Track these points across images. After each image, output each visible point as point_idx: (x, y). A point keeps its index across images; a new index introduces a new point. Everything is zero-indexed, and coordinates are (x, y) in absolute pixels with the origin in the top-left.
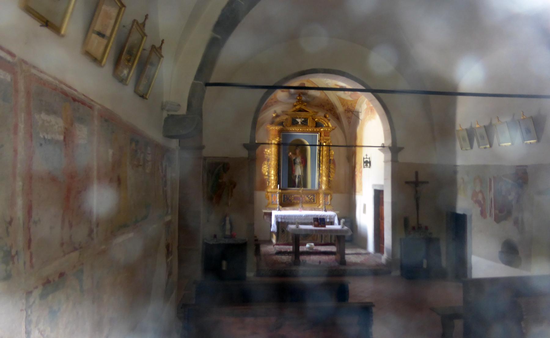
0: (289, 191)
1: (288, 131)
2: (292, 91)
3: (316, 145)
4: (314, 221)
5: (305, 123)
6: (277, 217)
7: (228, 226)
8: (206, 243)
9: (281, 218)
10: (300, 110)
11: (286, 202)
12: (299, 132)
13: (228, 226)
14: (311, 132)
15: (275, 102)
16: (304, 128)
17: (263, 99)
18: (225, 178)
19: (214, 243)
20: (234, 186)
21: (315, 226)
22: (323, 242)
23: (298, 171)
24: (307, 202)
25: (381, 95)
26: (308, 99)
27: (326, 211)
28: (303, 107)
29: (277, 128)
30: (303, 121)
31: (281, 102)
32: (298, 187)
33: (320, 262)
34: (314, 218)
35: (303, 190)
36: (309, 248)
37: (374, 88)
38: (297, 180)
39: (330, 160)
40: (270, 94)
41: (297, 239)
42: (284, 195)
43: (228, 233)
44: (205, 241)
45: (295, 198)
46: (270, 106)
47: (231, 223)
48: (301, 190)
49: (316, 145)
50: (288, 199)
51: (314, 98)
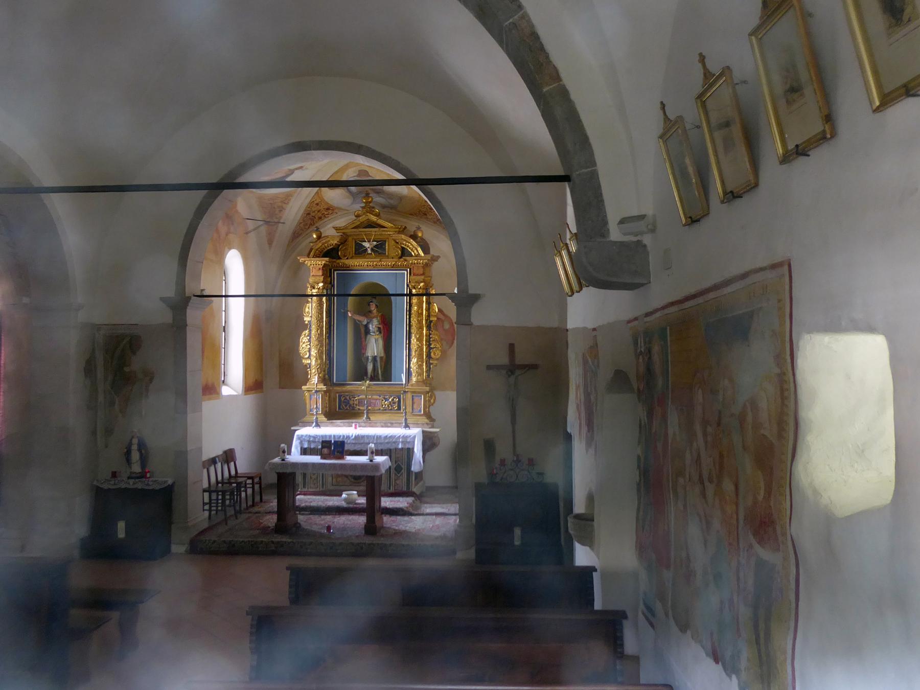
0: (348, 388)
1: (348, 268)
2: (353, 189)
3: (403, 295)
4: (323, 447)
5: (379, 249)
6: (300, 438)
7: (135, 456)
8: (98, 488)
9: (309, 441)
10: (372, 225)
11: (341, 409)
12: (375, 268)
13: (135, 456)
14: (394, 267)
15: (328, 209)
16: (375, 261)
17: (201, 211)
18: (136, 364)
19: (110, 487)
20: (151, 380)
21: (323, 458)
22: (392, 490)
23: (374, 347)
24: (385, 411)
25: (433, 188)
26: (392, 202)
27: (407, 426)
28: (374, 218)
29: (322, 262)
30: (375, 246)
31: (340, 209)
32: (372, 379)
33: (329, 528)
34: (323, 442)
35: (369, 385)
36: (345, 500)
37: (422, 176)
38: (370, 367)
39: (431, 322)
40: (216, 197)
41: (370, 482)
42: (340, 396)
43: (136, 468)
44: (95, 483)
45: (360, 402)
46: (427, 218)
47: (140, 450)
48: (382, 386)
49: (403, 295)
50: (347, 402)
51: (401, 198)
